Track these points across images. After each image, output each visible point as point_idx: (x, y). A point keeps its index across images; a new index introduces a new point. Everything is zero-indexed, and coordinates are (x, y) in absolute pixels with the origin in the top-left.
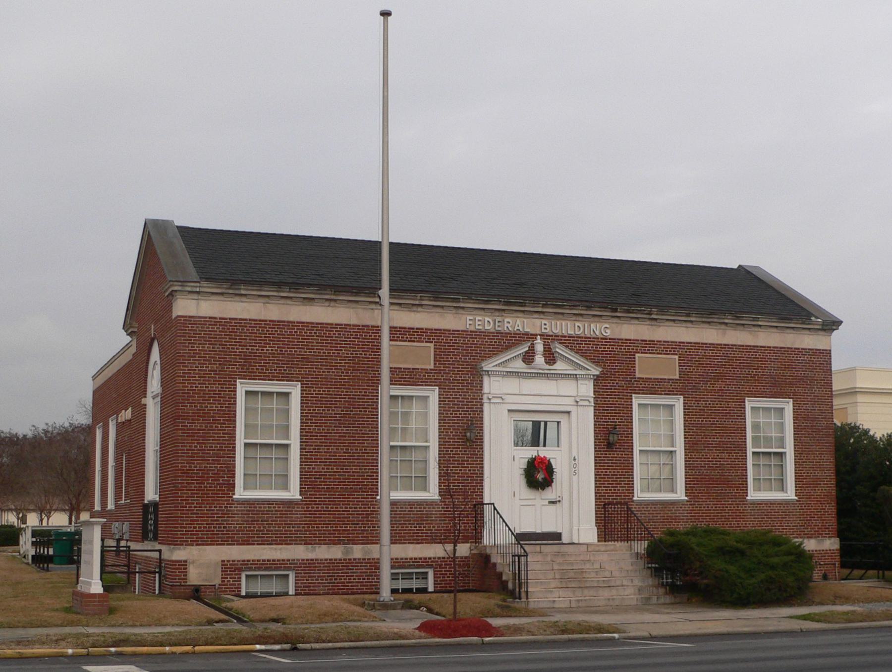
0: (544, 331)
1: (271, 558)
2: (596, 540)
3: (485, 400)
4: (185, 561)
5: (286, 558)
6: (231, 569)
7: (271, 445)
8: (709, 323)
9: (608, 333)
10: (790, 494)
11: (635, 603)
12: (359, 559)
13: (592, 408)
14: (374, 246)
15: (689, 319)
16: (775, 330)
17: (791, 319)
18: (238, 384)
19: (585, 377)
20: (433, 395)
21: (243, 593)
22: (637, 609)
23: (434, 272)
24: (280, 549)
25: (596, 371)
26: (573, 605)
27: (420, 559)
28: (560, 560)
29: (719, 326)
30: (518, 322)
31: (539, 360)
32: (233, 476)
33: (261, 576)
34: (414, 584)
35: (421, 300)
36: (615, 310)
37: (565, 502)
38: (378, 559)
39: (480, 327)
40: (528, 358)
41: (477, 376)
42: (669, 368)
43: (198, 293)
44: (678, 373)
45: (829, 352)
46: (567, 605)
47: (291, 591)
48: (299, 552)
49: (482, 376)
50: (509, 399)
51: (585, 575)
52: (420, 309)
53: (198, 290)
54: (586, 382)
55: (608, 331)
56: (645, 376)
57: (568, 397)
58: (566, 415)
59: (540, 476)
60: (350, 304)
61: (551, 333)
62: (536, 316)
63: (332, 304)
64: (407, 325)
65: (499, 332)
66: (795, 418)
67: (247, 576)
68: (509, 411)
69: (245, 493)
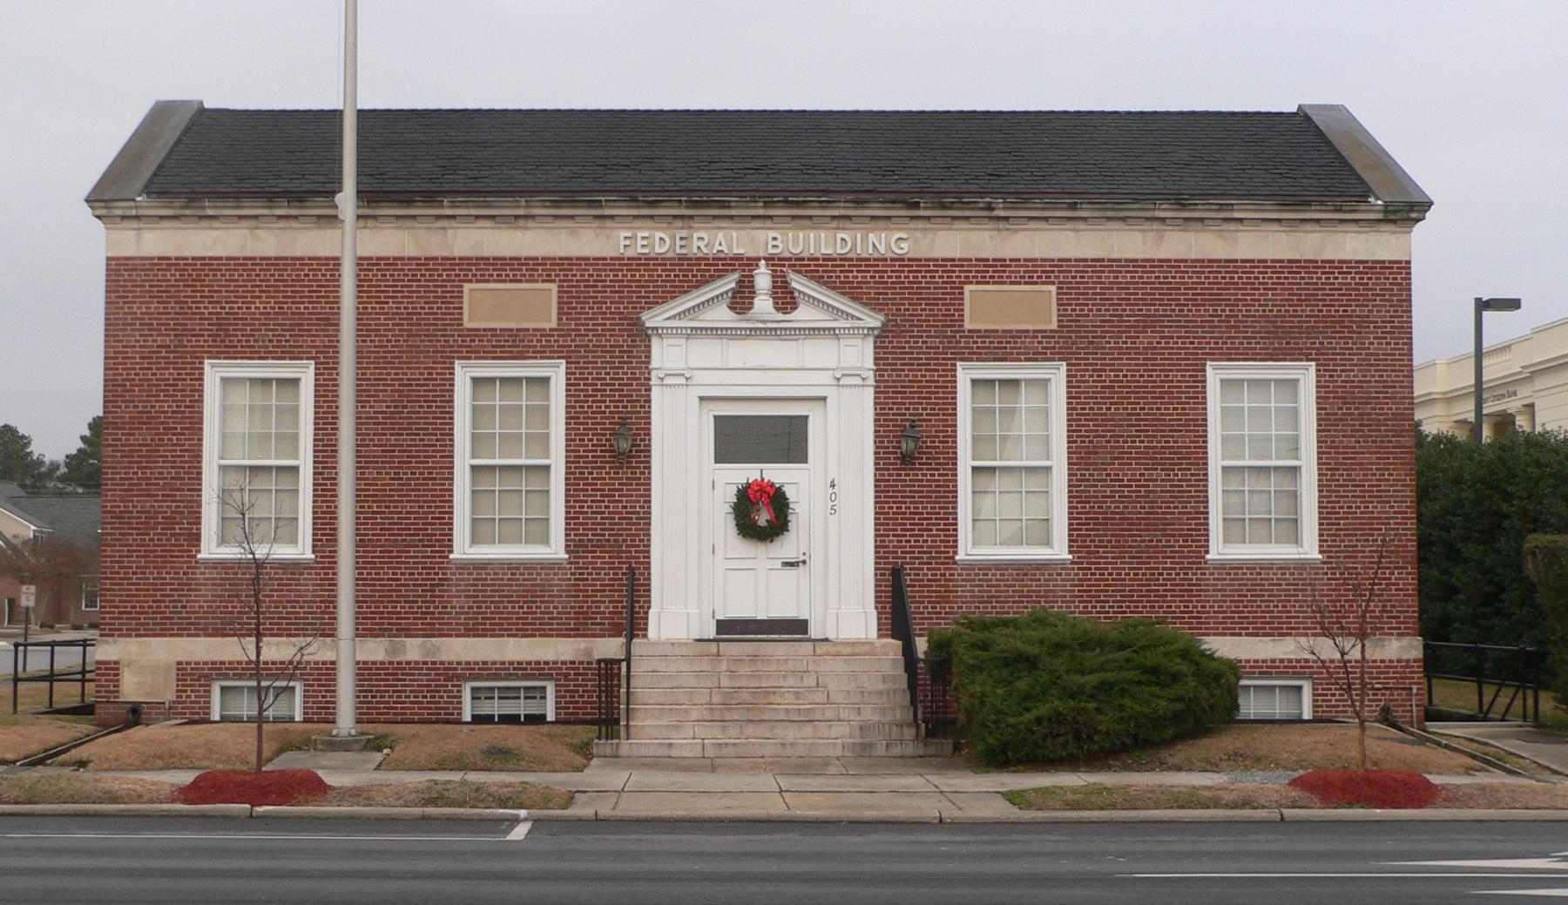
0: (771, 251)
2: (873, 633)
4: (116, 663)
6: (194, 677)
7: (268, 468)
8: (1124, 219)
9: (904, 249)
10: (1309, 549)
11: (839, 752)
12: (416, 663)
13: (872, 390)
14: (335, 116)
16: (1275, 227)
17: (1309, 203)
18: (959, 369)
19: (851, 333)
20: (1057, 376)
21: (216, 716)
23: (431, 158)
24: (277, 644)
25: (874, 320)
26: (710, 753)
27: (529, 663)
28: (745, 669)
29: (1147, 226)
30: (721, 235)
31: (763, 304)
32: (198, 521)
34: (521, 708)
35: (527, 207)
36: (916, 206)
37: (816, 563)
38: (333, 663)
39: (646, 251)
41: (637, 342)
42: (1039, 309)
43: (137, 217)
44: (1055, 318)
45: (1405, 266)
46: (697, 752)
47: (298, 717)
49: (649, 337)
50: (700, 377)
51: (772, 698)
52: (530, 224)
53: (134, 212)
54: (858, 342)
55: (904, 245)
56: (983, 327)
57: (826, 370)
58: (819, 405)
59: (763, 518)
60: (401, 223)
61: (787, 255)
62: (757, 224)
63: (370, 223)
64: (508, 254)
65: (683, 258)
66: (1321, 400)
67: (223, 689)
68: (702, 399)
69: (473, 550)
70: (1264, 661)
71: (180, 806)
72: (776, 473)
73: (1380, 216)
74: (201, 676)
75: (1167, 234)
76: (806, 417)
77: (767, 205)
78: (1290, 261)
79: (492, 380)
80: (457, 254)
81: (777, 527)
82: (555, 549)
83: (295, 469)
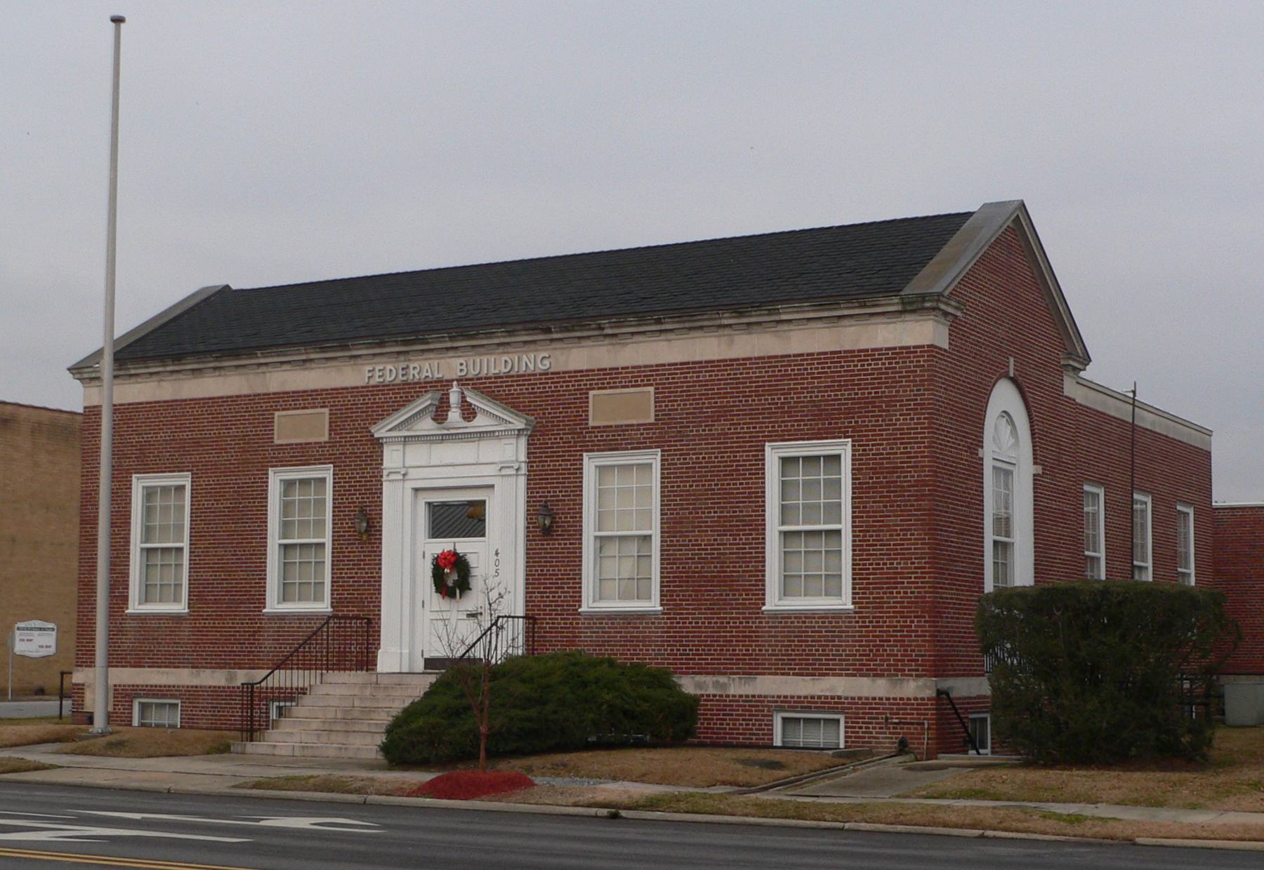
1: (158, 683)
3: (524, 470)
5: (171, 683)
15: (663, 327)
16: (819, 324)
18: (134, 480)
22: (372, 767)
26: (297, 753)
31: (454, 415)
33: (805, 720)
36: (548, 331)
40: (440, 415)
42: (639, 406)
47: (842, 746)
48: (183, 677)
51: (373, 716)
55: (547, 362)
57: (493, 462)
59: (452, 578)
60: (239, 371)
62: (451, 354)
64: (301, 388)
65: (405, 383)
67: (784, 719)
68: (416, 490)
70: (806, 697)
71: (428, 801)
72: (464, 546)
73: (899, 308)
74: (127, 695)
75: (736, 338)
76: (483, 502)
77: (452, 339)
78: (832, 353)
79: (796, 459)
80: (271, 390)
81: (463, 585)
82: (844, 601)
83: (838, 532)
